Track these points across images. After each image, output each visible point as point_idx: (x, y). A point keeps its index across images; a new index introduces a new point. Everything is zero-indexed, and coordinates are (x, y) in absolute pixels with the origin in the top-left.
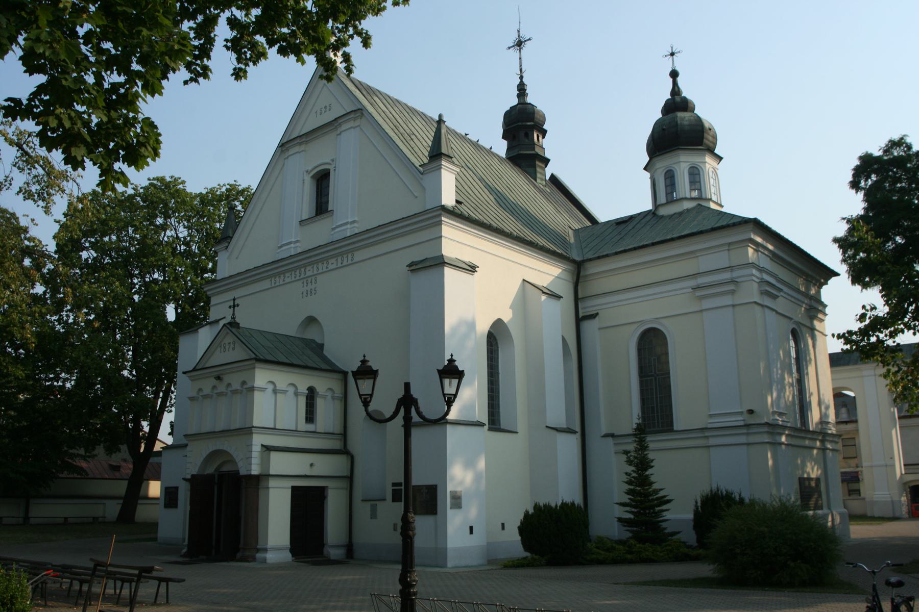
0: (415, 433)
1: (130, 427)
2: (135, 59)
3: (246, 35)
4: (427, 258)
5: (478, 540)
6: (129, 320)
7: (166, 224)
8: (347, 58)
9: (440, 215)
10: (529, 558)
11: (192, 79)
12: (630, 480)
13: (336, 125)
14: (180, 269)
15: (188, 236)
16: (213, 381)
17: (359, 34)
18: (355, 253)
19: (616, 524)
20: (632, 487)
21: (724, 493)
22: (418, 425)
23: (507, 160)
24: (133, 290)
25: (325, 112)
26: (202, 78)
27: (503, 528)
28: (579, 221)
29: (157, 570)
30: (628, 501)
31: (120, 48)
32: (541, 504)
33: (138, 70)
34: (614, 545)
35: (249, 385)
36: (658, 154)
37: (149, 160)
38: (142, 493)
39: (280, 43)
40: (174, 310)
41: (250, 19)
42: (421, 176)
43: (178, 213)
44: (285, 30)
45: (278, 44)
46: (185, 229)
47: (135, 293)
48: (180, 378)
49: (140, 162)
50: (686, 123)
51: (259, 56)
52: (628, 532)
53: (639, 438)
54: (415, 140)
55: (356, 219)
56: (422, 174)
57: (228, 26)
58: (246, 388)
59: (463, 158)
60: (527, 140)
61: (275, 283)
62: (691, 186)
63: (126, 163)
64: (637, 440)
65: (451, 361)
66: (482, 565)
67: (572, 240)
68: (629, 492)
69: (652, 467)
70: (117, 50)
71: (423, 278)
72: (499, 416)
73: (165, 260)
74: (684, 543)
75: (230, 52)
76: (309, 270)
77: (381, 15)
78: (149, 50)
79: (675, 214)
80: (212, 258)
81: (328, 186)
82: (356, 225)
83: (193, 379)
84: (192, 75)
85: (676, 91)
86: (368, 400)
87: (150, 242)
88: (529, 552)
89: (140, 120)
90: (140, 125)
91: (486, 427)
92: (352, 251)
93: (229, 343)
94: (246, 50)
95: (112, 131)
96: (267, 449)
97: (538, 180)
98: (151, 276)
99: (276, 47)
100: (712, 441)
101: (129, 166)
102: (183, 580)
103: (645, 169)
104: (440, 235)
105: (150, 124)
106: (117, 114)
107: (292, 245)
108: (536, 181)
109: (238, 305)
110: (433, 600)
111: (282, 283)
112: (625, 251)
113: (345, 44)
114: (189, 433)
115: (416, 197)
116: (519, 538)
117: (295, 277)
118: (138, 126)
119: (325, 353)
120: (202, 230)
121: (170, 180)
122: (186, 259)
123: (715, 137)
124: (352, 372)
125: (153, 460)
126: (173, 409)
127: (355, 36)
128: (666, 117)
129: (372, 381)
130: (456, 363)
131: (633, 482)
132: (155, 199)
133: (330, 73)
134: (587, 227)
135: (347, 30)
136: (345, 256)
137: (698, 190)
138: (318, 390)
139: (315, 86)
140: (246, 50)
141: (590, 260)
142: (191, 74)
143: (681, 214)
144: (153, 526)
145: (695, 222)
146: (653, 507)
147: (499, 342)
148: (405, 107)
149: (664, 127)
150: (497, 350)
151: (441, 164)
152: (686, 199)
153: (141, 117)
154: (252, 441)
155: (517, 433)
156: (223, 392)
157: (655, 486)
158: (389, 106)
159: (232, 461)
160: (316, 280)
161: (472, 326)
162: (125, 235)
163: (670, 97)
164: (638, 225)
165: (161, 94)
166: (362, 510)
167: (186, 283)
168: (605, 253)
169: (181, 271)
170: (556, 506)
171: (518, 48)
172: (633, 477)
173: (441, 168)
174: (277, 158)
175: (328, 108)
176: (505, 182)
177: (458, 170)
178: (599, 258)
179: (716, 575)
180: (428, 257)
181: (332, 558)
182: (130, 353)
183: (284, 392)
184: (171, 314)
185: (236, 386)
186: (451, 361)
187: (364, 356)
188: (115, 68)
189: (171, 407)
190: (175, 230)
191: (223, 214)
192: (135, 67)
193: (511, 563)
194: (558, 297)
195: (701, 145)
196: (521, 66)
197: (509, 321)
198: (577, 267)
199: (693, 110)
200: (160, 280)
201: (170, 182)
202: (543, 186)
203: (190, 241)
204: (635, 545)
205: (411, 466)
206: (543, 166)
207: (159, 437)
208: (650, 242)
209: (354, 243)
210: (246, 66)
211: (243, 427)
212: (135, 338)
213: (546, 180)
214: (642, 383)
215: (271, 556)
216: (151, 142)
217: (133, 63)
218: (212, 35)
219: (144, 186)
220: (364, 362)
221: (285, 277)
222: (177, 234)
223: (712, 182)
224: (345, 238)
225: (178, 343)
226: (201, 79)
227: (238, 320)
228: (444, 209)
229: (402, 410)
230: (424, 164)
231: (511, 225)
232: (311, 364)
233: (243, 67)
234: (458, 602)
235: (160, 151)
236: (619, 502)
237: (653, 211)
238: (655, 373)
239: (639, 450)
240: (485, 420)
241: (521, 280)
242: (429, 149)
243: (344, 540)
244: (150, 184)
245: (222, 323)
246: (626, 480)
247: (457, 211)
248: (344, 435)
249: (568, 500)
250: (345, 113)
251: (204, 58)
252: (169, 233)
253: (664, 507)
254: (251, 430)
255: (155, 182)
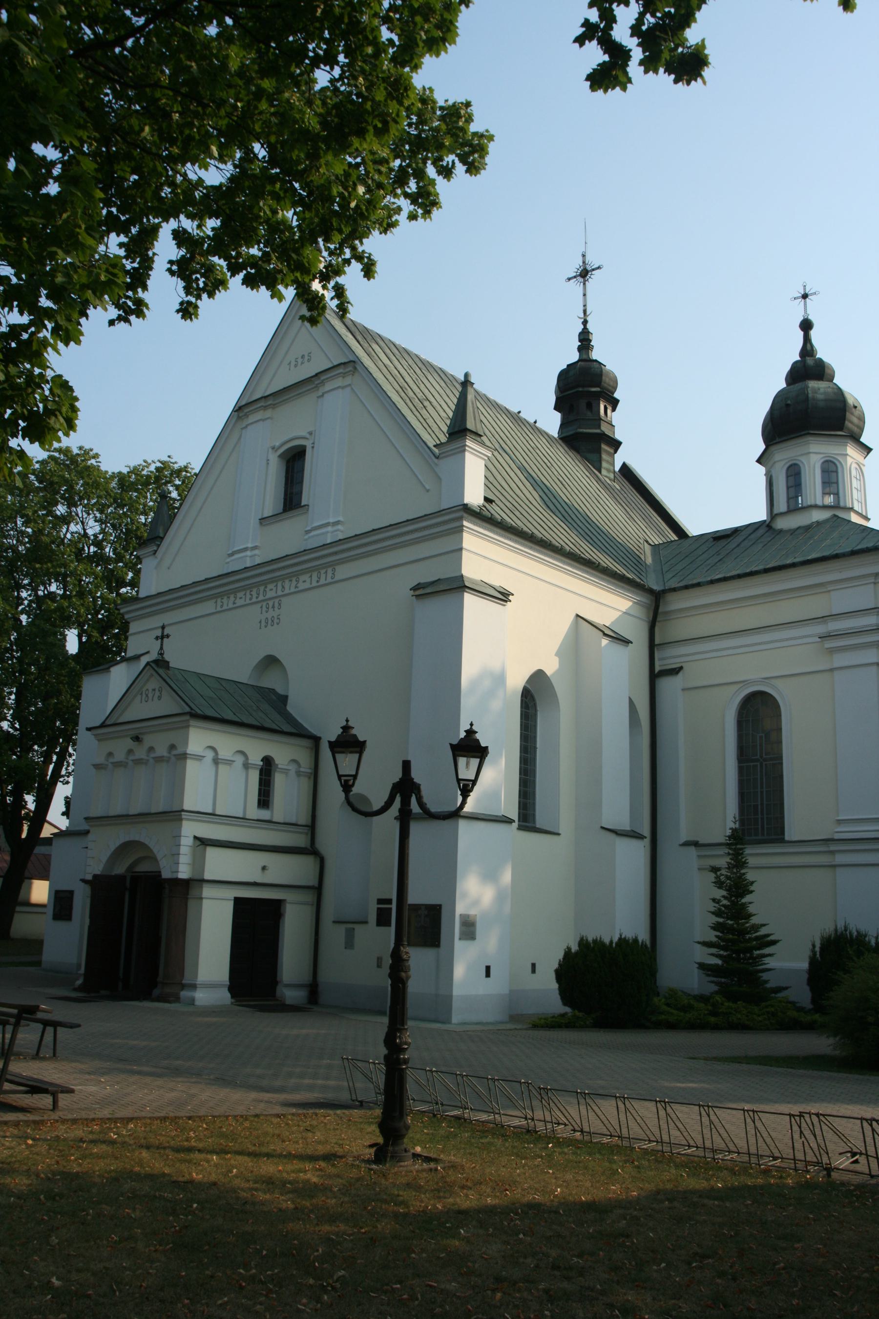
0: (416, 830)
1: (8, 802)
2: (45, 292)
3: (199, 254)
4: (439, 580)
5: (497, 986)
6: (13, 650)
7: (70, 514)
8: (340, 292)
9: (461, 518)
10: (569, 1015)
11: (120, 318)
12: (720, 909)
13: (316, 383)
14: (87, 580)
15: (100, 534)
16: (129, 743)
17: (359, 257)
18: (338, 568)
19: (695, 971)
20: (721, 920)
21: (855, 934)
22: (418, 818)
23: (560, 442)
24: (20, 608)
25: (302, 363)
26: (134, 316)
27: (534, 970)
28: (661, 533)
29: (44, 1011)
30: (714, 939)
31: (24, 276)
32: (590, 939)
33: (48, 307)
34: (692, 1002)
35: (179, 750)
36: (778, 440)
37: (60, 434)
38: (22, 896)
39: (246, 269)
40: (77, 638)
41: (204, 232)
42: (436, 460)
43: (88, 500)
44: (254, 251)
45: (245, 272)
46: (97, 524)
47: (22, 612)
48: (82, 736)
49: (49, 437)
50: (820, 397)
51: (215, 285)
52: (713, 985)
53: (735, 850)
54: (430, 408)
55: (341, 519)
56: (437, 458)
57: (174, 242)
58: (175, 755)
59: (497, 436)
60: (589, 413)
61: (222, 606)
62: (823, 488)
63: (27, 439)
64: (731, 852)
65: (470, 732)
66: (502, 1023)
67: (649, 561)
68: (716, 927)
69: (752, 892)
70: (20, 279)
71: (434, 607)
72: (534, 810)
73: (65, 565)
74: (793, 1003)
75: (175, 278)
76: (271, 590)
77: (391, 232)
78: (64, 280)
79: (799, 528)
80: (133, 566)
81: (302, 470)
82: (340, 527)
83: (100, 739)
84: (121, 312)
85: (807, 350)
86: (351, 783)
87: (45, 539)
88: (569, 1006)
89: (49, 378)
90: (48, 386)
91: (515, 825)
92: (333, 565)
93: (154, 690)
94: (198, 276)
95: (10, 393)
96: (202, 842)
97: (604, 472)
98: (45, 588)
99: (241, 275)
100: (840, 859)
101: (32, 442)
102: (79, 1026)
103: (759, 461)
104: (459, 547)
105: (63, 385)
106: (17, 370)
107: (249, 553)
108: (600, 472)
109: (168, 636)
110: (431, 1071)
111: (231, 606)
112: (725, 579)
113: (338, 272)
114: (91, 815)
115: (428, 491)
116: (556, 986)
117: (251, 599)
118: (46, 388)
119: (289, 708)
120: (120, 525)
121: (79, 452)
122: (97, 566)
123: (862, 419)
124: (329, 742)
125: (39, 850)
126: (71, 779)
127: (353, 261)
128: (792, 386)
129: (357, 755)
130: (478, 736)
131: (723, 912)
132: (56, 479)
133: (315, 313)
134: (672, 541)
135: (342, 252)
136: (323, 571)
137: (833, 494)
138: (277, 762)
139: (308, 390)
140: (198, 276)
141: (674, 590)
142: (119, 310)
143: (807, 528)
144: (35, 945)
145: (828, 542)
146: (750, 950)
147: (538, 702)
148: (417, 360)
149: (789, 402)
150: (535, 715)
151: (466, 445)
152: (816, 506)
153: (49, 374)
154: (180, 831)
155: (558, 834)
156: (142, 759)
157: (754, 920)
158: (393, 358)
159: (153, 859)
160: (280, 604)
161: (500, 679)
162: (12, 529)
163: (798, 358)
164: (746, 541)
165: (78, 342)
166: (333, 936)
167: (95, 599)
168: (695, 581)
169: (89, 582)
170: (611, 942)
171: (582, 280)
172: (724, 906)
173: (464, 451)
174: (230, 427)
175: (306, 358)
176: (556, 473)
177: (489, 454)
178: (687, 587)
179: (837, 1052)
180: (442, 577)
181: (288, 1002)
182: (13, 697)
183: (229, 762)
184: (72, 645)
185: (161, 751)
186: (470, 732)
187: (347, 721)
188: (15, 303)
189: (68, 777)
190: (83, 523)
191: (151, 504)
192: (45, 302)
193: (543, 1021)
194: (626, 642)
195: (841, 429)
196: (585, 306)
197: (553, 675)
198: (654, 598)
199: (832, 377)
200: (59, 594)
201: (78, 454)
202: (610, 480)
203: (103, 540)
204: (722, 1004)
205: (407, 879)
206: (612, 451)
207: (49, 818)
208: (761, 567)
209: (336, 553)
210: (197, 300)
211: (169, 810)
212: (21, 675)
213: (614, 472)
214: (741, 770)
215: (201, 995)
216: (64, 410)
217: (41, 297)
218: (150, 253)
219: (40, 459)
220: (346, 728)
221: (236, 598)
222: (85, 530)
223: (855, 483)
224: (324, 545)
225: (80, 687)
226: (133, 318)
227: (167, 657)
228: (467, 510)
229: (398, 799)
230: (442, 443)
231: (563, 537)
232: (268, 724)
233: (193, 300)
234: (466, 1076)
235: (76, 422)
236: (701, 940)
237: (767, 522)
238: (761, 757)
239: (733, 868)
240: (514, 814)
241: (573, 616)
242: (448, 422)
243: (305, 977)
244: (50, 457)
245: (144, 660)
246: (713, 909)
247: (486, 513)
248: (312, 827)
249: (629, 934)
250: (330, 365)
251: (137, 288)
252: (73, 528)
253: (766, 951)
254: (181, 815)
255: (56, 454)
